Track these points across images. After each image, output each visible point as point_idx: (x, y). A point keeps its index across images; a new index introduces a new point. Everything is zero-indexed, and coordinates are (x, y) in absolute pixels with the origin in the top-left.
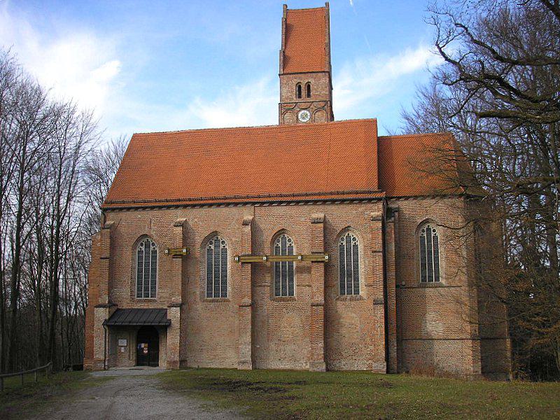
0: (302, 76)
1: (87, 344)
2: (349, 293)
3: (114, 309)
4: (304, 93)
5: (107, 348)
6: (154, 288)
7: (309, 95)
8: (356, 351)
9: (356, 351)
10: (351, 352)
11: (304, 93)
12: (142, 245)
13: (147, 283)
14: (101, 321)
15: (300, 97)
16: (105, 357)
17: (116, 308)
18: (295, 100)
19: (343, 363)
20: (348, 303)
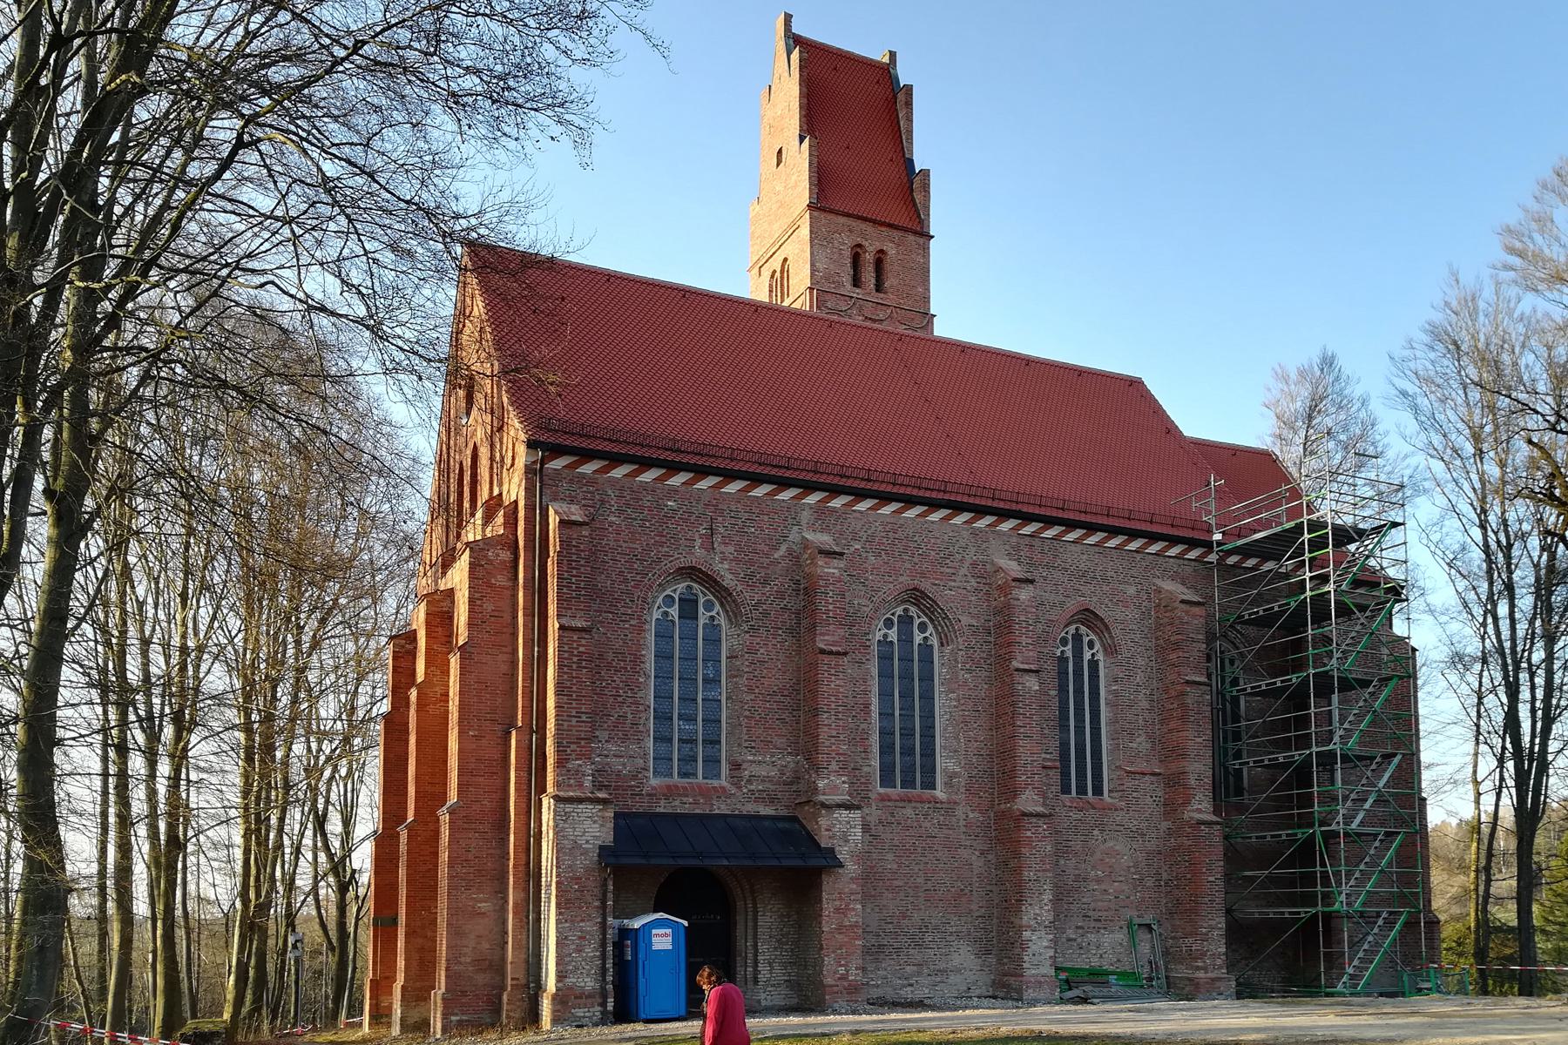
4: (869, 276)
11: (869, 276)
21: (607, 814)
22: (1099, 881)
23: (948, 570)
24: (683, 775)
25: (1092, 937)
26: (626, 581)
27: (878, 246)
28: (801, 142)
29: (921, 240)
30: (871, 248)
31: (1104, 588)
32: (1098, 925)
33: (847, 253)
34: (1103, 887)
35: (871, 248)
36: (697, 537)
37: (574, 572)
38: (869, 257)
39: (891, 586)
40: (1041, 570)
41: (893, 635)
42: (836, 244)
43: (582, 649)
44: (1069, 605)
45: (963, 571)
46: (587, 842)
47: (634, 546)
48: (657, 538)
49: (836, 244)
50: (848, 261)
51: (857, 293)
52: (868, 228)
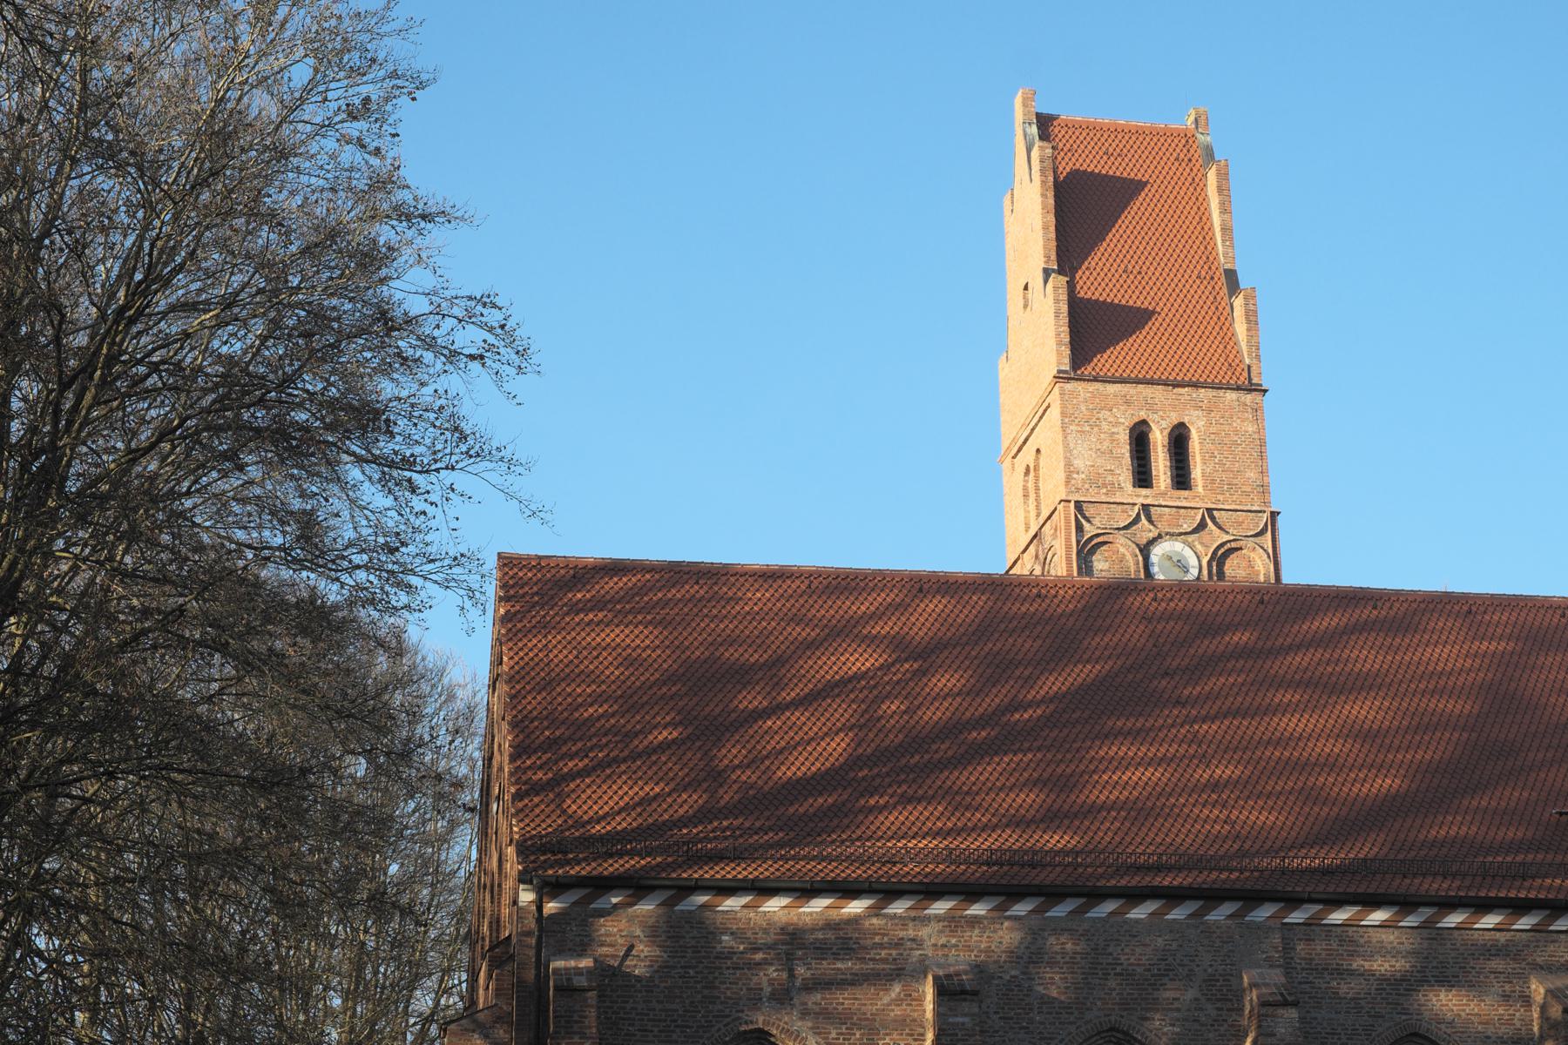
27: (1174, 418)
28: (1046, 282)
29: (1248, 398)
33: (1124, 437)
38: (1159, 439)
39: (1072, 1028)
42: (1105, 426)
44: (1380, 1030)
47: (673, 1006)
48: (706, 992)
49: (1105, 426)
50: (1125, 450)
51: (1144, 496)
52: (1157, 393)
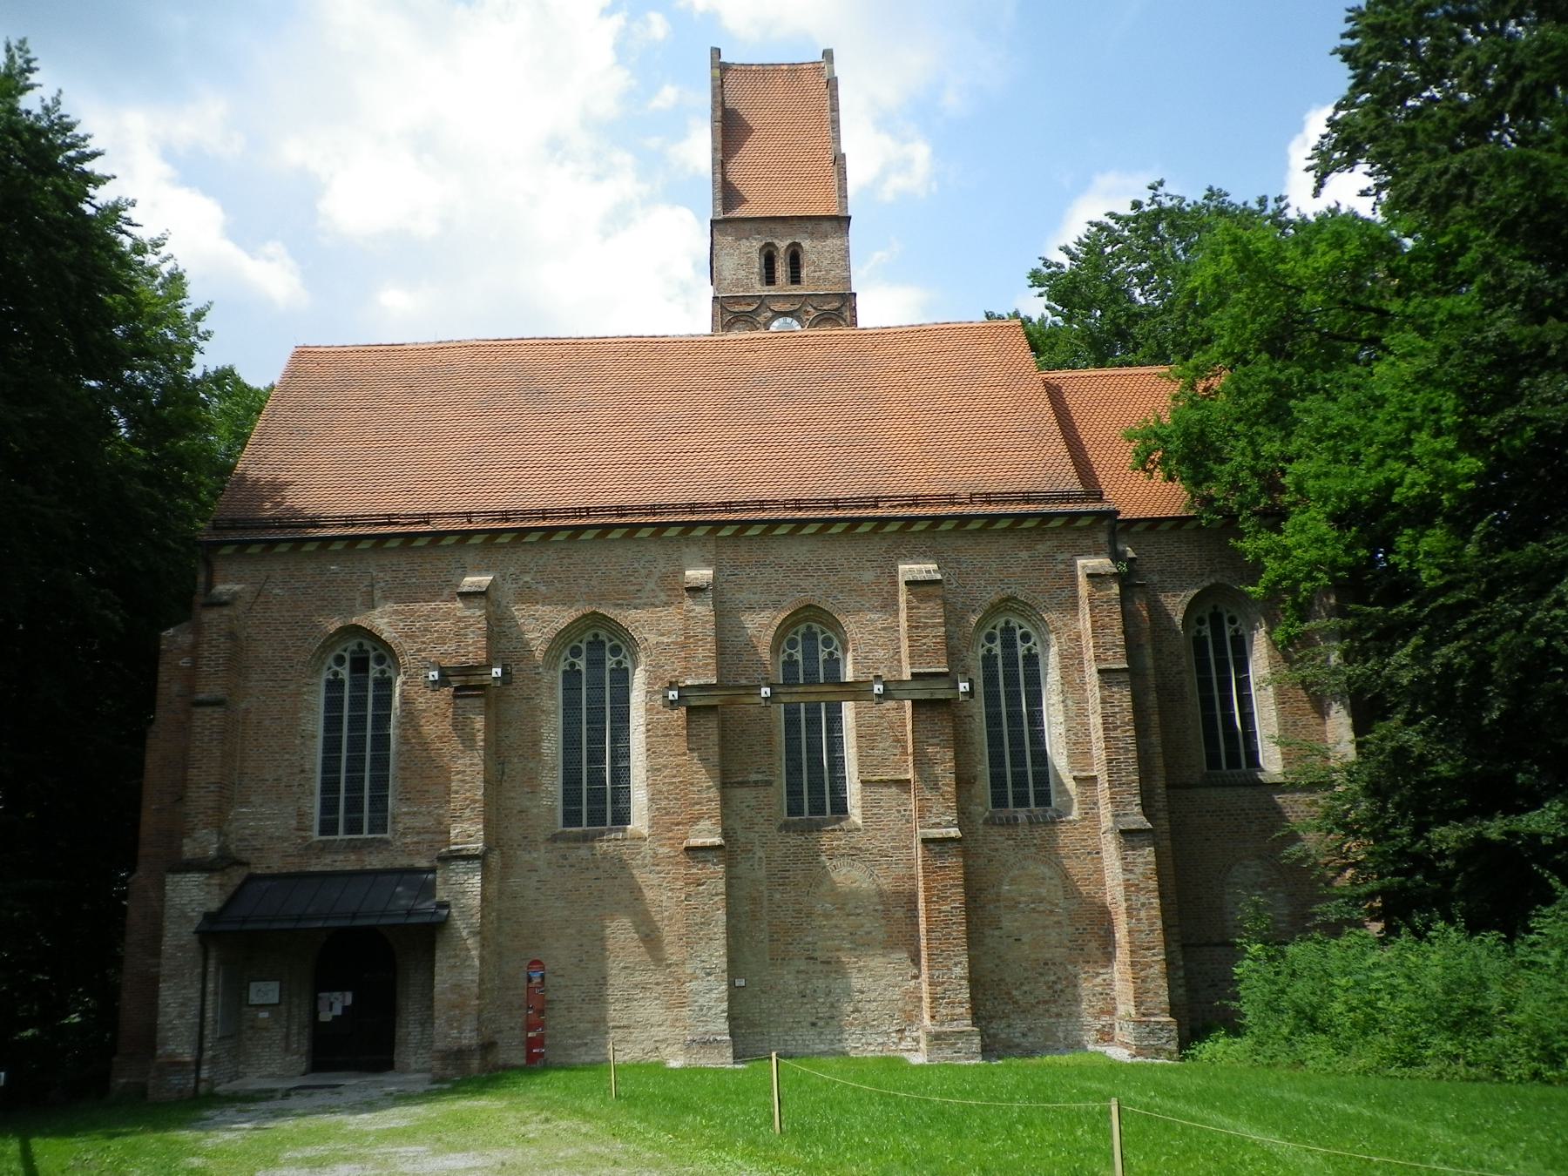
0: (779, 227)
1: (351, 1081)
2: (1021, 801)
3: (237, 876)
4: (782, 271)
5: (209, 1014)
6: (379, 801)
7: (795, 279)
8: (1059, 987)
9: (1059, 987)
10: (1042, 991)
11: (782, 271)
12: (340, 660)
13: (355, 785)
14: (191, 920)
15: (770, 279)
16: (201, 1049)
17: (244, 872)
18: (761, 290)
19: (1021, 1026)
20: (1022, 832)
21: (213, 882)
22: (827, 916)
23: (632, 588)
24: (349, 831)
25: (820, 984)
26: (287, 648)
30: (782, 245)
31: (832, 579)
32: (826, 968)
34: (833, 922)
35: (782, 245)
36: (358, 594)
37: (214, 650)
40: (748, 571)
41: (997, 649)
43: (214, 722)
45: (651, 585)
46: (193, 910)
